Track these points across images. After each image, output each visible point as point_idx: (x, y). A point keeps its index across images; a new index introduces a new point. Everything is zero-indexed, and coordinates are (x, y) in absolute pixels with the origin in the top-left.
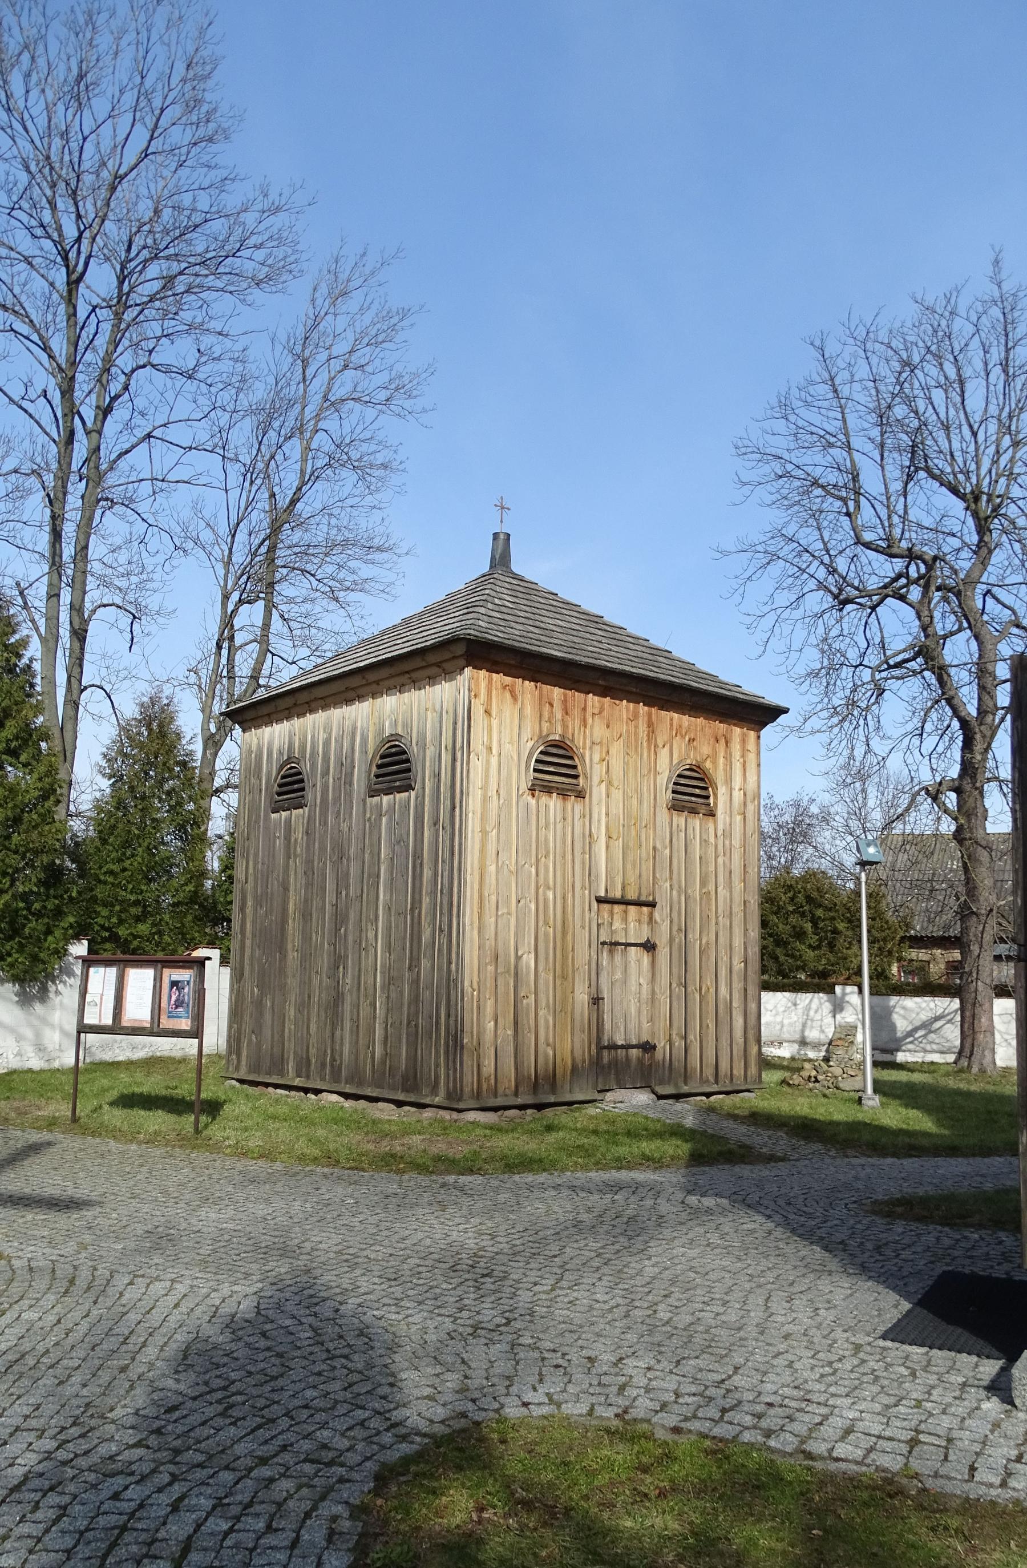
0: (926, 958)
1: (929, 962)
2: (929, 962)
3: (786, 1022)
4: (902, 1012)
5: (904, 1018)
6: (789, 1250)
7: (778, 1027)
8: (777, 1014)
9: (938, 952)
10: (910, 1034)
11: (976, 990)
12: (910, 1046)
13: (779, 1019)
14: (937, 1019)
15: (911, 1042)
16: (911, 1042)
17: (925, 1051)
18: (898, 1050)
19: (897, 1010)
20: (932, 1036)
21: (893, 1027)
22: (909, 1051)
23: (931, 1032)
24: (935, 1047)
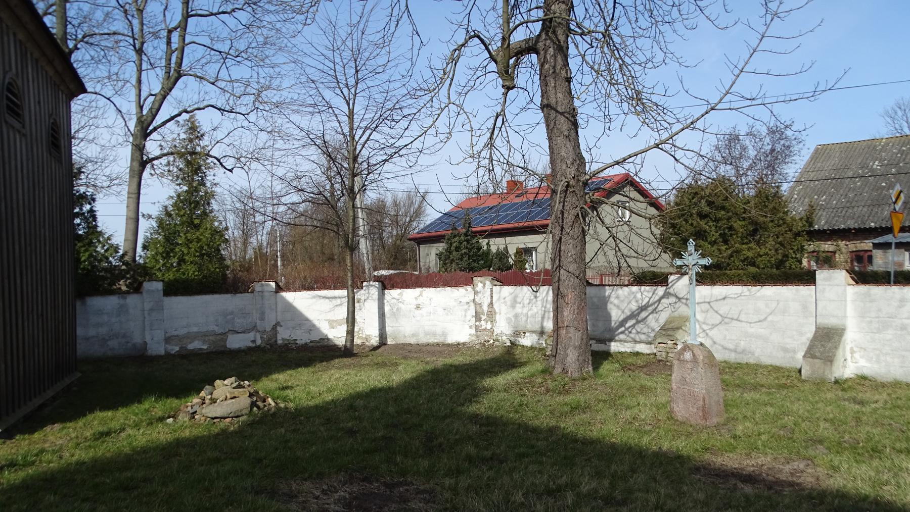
0: (832, 248)
1: (834, 253)
2: (834, 253)
3: (530, 314)
4: (616, 301)
5: (618, 307)
6: (752, 469)
7: (524, 319)
8: (524, 306)
9: (842, 244)
10: (622, 323)
11: (559, 280)
12: (622, 337)
13: (525, 311)
14: (643, 309)
15: (622, 333)
16: (622, 333)
17: (635, 341)
18: (611, 340)
19: (612, 299)
20: (639, 327)
21: (608, 317)
22: (620, 341)
23: (638, 322)
24: (643, 337)
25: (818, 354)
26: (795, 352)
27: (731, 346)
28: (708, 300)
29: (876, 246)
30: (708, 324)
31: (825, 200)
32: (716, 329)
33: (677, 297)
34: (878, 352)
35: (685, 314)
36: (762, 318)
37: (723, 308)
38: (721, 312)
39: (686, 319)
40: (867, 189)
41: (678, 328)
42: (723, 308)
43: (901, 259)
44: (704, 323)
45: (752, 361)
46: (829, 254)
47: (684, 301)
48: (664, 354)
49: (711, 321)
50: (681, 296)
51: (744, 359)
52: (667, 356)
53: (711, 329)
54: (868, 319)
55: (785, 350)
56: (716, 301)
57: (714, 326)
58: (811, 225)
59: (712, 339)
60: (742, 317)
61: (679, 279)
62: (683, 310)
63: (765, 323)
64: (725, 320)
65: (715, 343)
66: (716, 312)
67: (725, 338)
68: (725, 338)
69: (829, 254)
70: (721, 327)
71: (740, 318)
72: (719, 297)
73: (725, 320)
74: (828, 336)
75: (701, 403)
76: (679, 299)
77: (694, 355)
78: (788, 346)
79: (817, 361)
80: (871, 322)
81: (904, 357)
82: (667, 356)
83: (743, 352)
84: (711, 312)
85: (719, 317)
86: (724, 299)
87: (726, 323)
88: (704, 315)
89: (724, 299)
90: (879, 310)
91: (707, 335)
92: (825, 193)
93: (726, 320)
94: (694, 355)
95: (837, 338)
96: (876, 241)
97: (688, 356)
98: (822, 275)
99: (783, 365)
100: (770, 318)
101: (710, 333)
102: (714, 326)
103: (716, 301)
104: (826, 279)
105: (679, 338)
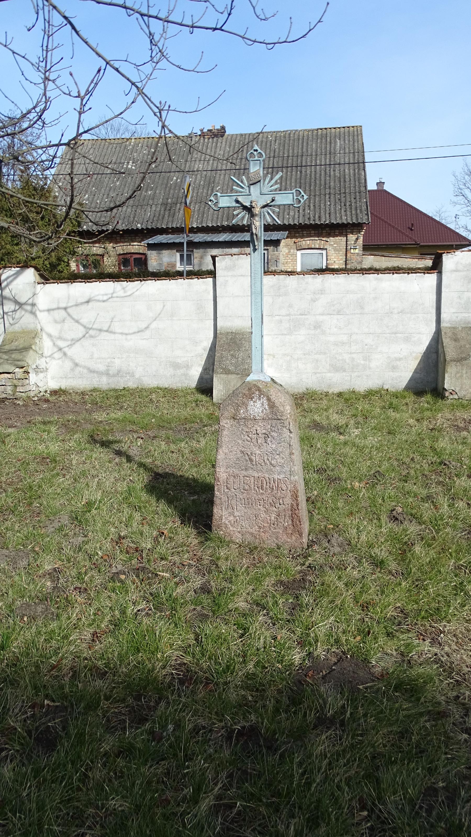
0: (100, 251)
1: (103, 256)
2: (103, 256)
25: (232, 368)
26: (188, 367)
27: (102, 368)
28: (64, 305)
29: (151, 247)
30: (65, 340)
31: (88, 199)
32: (78, 344)
33: (16, 302)
34: (288, 358)
35: (31, 326)
36: (144, 326)
37: (87, 315)
38: (84, 321)
39: (33, 335)
40: (126, 189)
41: (27, 348)
42: (87, 315)
43: (173, 260)
44: (60, 338)
45: (132, 385)
46: (98, 258)
47: (28, 308)
48: (9, 390)
49: (71, 335)
50: (22, 300)
51: (120, 383)
52: (14, 392)
53: (70, 346)
54: (277, 318)
55: (176, 366)
56: (76, 305)
57: (74, 341)
58: (79, 225)
59: (72, 360)
60: (116, 327)
61: (17, 275)
62: (25, 321)
63: (148, 333)
64: (89, 332)
65: (76, 365)
66: (77, 322)
67: (92, 357)
68: (92, 357)
69: (98, 258)
70: (87, 343)
71: (112, 329)
72: (80, 300)
73: (89, 332)
74: (235, 342)
75: (288, 501)
76: (21, 305)
77: (272, 405)
78: (179, 361)
79: (233, 376)
80: (281, 321)
81: (317, 361)
82: (14, 392)
83: (119, 373)
84: (69, 323)
85: (81, 328)
86: (88, 302)
87: (91, 337)
88: (59, 326)
89: (88, 302)
90: (290, 306)
91: (65, 354)
92: (87, 192)
93: (91, 332)
94: (272, 405)
95: (246, 344)
96: (151, 241)
97: (257, 407)
98: (224, 263)
99: (174, 386)
100: (154, 325)
101: (69, 352)
102: (74, 341)
103: (76, 305)
104: (227, 268)
105: (30, 362)
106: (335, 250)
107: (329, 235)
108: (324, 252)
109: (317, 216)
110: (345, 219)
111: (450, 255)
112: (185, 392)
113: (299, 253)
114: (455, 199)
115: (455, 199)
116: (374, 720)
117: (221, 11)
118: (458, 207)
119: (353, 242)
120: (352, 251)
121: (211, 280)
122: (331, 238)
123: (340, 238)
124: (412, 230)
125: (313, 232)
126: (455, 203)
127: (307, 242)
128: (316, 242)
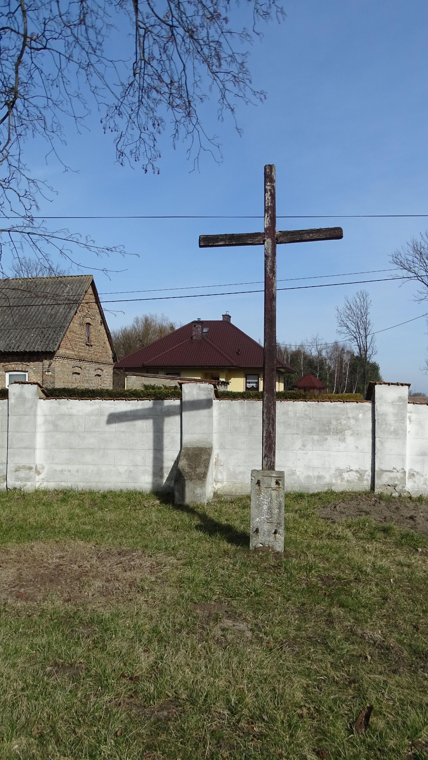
106: (35, 372)
107: (29, 361)
108: (27, 374)
109: (17, 345)
110: (38, 348)
111: (383, 378)
112: (129, 499)
113: (7, 375)
114: (340, 329)
115: (340, 329)
116: (407, 682)
117: (255, 30)
118: (343, 335)
119: (47, 366)
120: (47, 373)
121: (368, 405)
122: (31, 363)
123: (37, 363)
124: (238, 354)
125: (16, 358)
126: (340, 332)
127: (12, 365)
128: (19, 366)
